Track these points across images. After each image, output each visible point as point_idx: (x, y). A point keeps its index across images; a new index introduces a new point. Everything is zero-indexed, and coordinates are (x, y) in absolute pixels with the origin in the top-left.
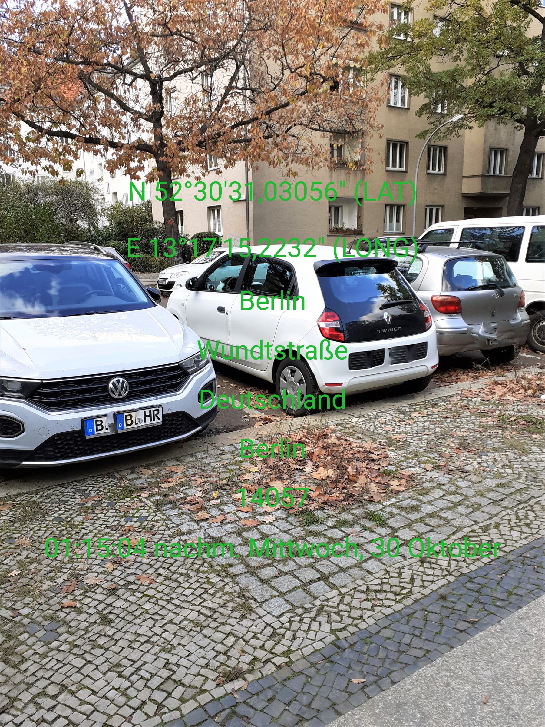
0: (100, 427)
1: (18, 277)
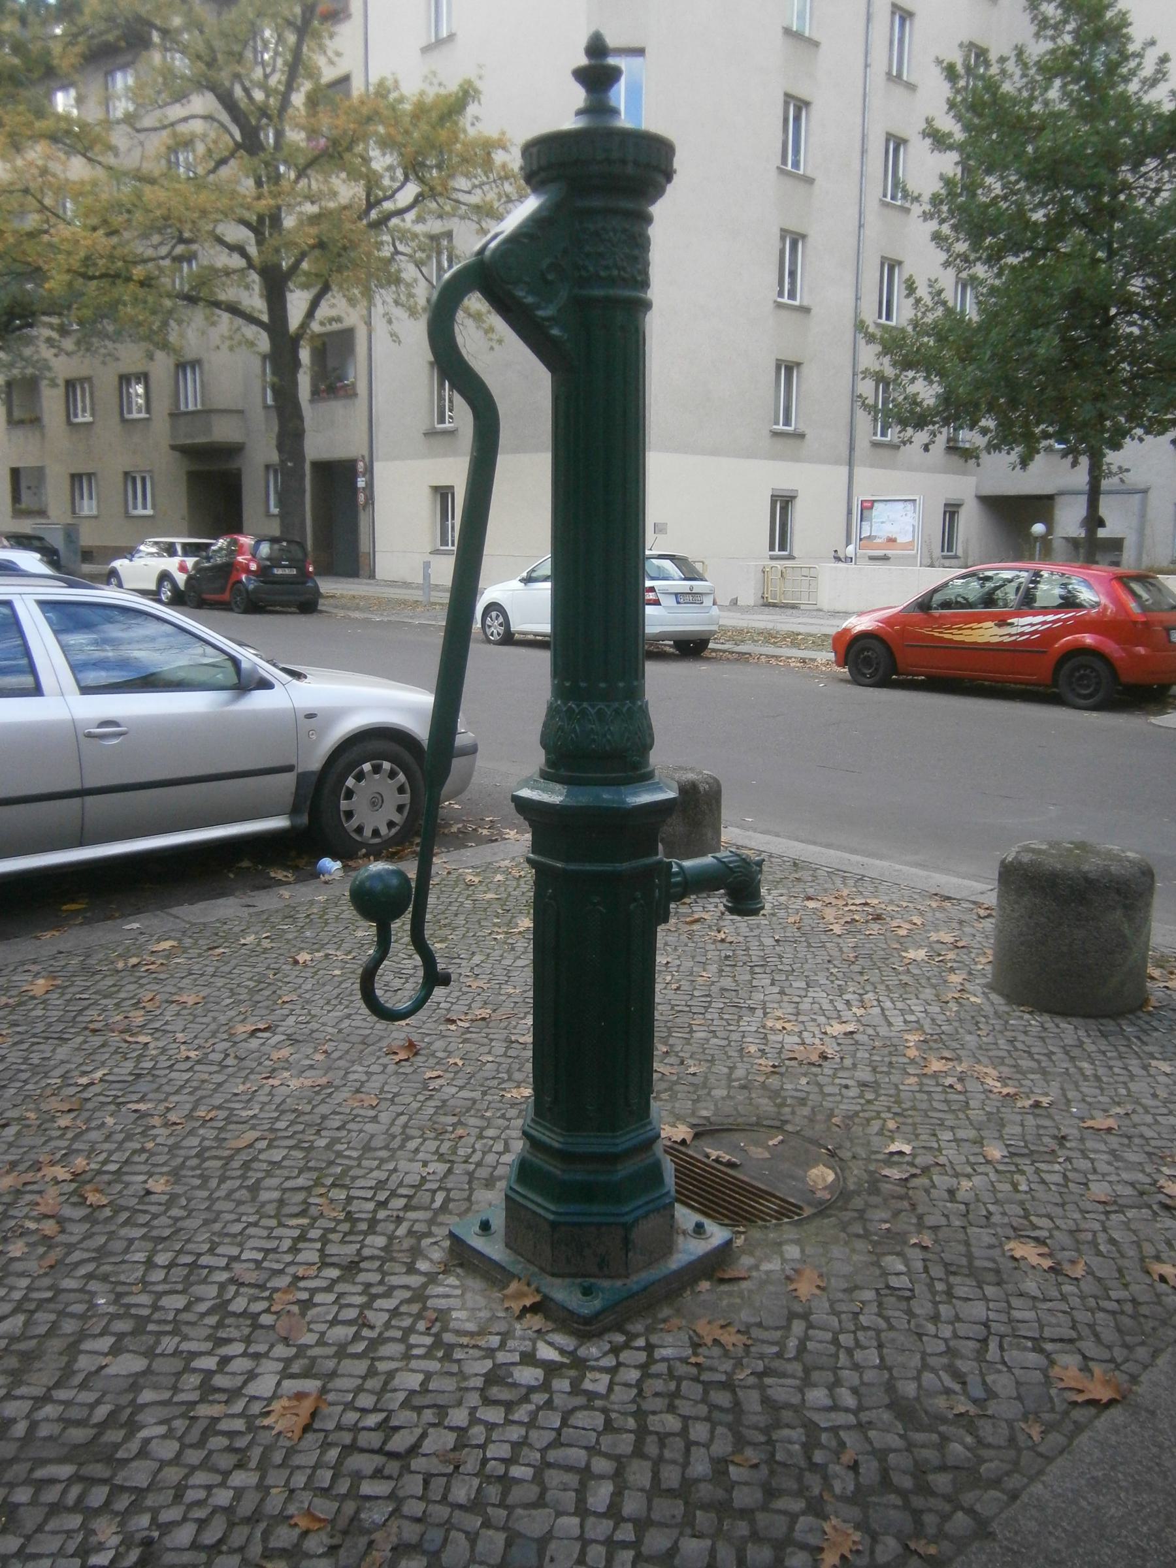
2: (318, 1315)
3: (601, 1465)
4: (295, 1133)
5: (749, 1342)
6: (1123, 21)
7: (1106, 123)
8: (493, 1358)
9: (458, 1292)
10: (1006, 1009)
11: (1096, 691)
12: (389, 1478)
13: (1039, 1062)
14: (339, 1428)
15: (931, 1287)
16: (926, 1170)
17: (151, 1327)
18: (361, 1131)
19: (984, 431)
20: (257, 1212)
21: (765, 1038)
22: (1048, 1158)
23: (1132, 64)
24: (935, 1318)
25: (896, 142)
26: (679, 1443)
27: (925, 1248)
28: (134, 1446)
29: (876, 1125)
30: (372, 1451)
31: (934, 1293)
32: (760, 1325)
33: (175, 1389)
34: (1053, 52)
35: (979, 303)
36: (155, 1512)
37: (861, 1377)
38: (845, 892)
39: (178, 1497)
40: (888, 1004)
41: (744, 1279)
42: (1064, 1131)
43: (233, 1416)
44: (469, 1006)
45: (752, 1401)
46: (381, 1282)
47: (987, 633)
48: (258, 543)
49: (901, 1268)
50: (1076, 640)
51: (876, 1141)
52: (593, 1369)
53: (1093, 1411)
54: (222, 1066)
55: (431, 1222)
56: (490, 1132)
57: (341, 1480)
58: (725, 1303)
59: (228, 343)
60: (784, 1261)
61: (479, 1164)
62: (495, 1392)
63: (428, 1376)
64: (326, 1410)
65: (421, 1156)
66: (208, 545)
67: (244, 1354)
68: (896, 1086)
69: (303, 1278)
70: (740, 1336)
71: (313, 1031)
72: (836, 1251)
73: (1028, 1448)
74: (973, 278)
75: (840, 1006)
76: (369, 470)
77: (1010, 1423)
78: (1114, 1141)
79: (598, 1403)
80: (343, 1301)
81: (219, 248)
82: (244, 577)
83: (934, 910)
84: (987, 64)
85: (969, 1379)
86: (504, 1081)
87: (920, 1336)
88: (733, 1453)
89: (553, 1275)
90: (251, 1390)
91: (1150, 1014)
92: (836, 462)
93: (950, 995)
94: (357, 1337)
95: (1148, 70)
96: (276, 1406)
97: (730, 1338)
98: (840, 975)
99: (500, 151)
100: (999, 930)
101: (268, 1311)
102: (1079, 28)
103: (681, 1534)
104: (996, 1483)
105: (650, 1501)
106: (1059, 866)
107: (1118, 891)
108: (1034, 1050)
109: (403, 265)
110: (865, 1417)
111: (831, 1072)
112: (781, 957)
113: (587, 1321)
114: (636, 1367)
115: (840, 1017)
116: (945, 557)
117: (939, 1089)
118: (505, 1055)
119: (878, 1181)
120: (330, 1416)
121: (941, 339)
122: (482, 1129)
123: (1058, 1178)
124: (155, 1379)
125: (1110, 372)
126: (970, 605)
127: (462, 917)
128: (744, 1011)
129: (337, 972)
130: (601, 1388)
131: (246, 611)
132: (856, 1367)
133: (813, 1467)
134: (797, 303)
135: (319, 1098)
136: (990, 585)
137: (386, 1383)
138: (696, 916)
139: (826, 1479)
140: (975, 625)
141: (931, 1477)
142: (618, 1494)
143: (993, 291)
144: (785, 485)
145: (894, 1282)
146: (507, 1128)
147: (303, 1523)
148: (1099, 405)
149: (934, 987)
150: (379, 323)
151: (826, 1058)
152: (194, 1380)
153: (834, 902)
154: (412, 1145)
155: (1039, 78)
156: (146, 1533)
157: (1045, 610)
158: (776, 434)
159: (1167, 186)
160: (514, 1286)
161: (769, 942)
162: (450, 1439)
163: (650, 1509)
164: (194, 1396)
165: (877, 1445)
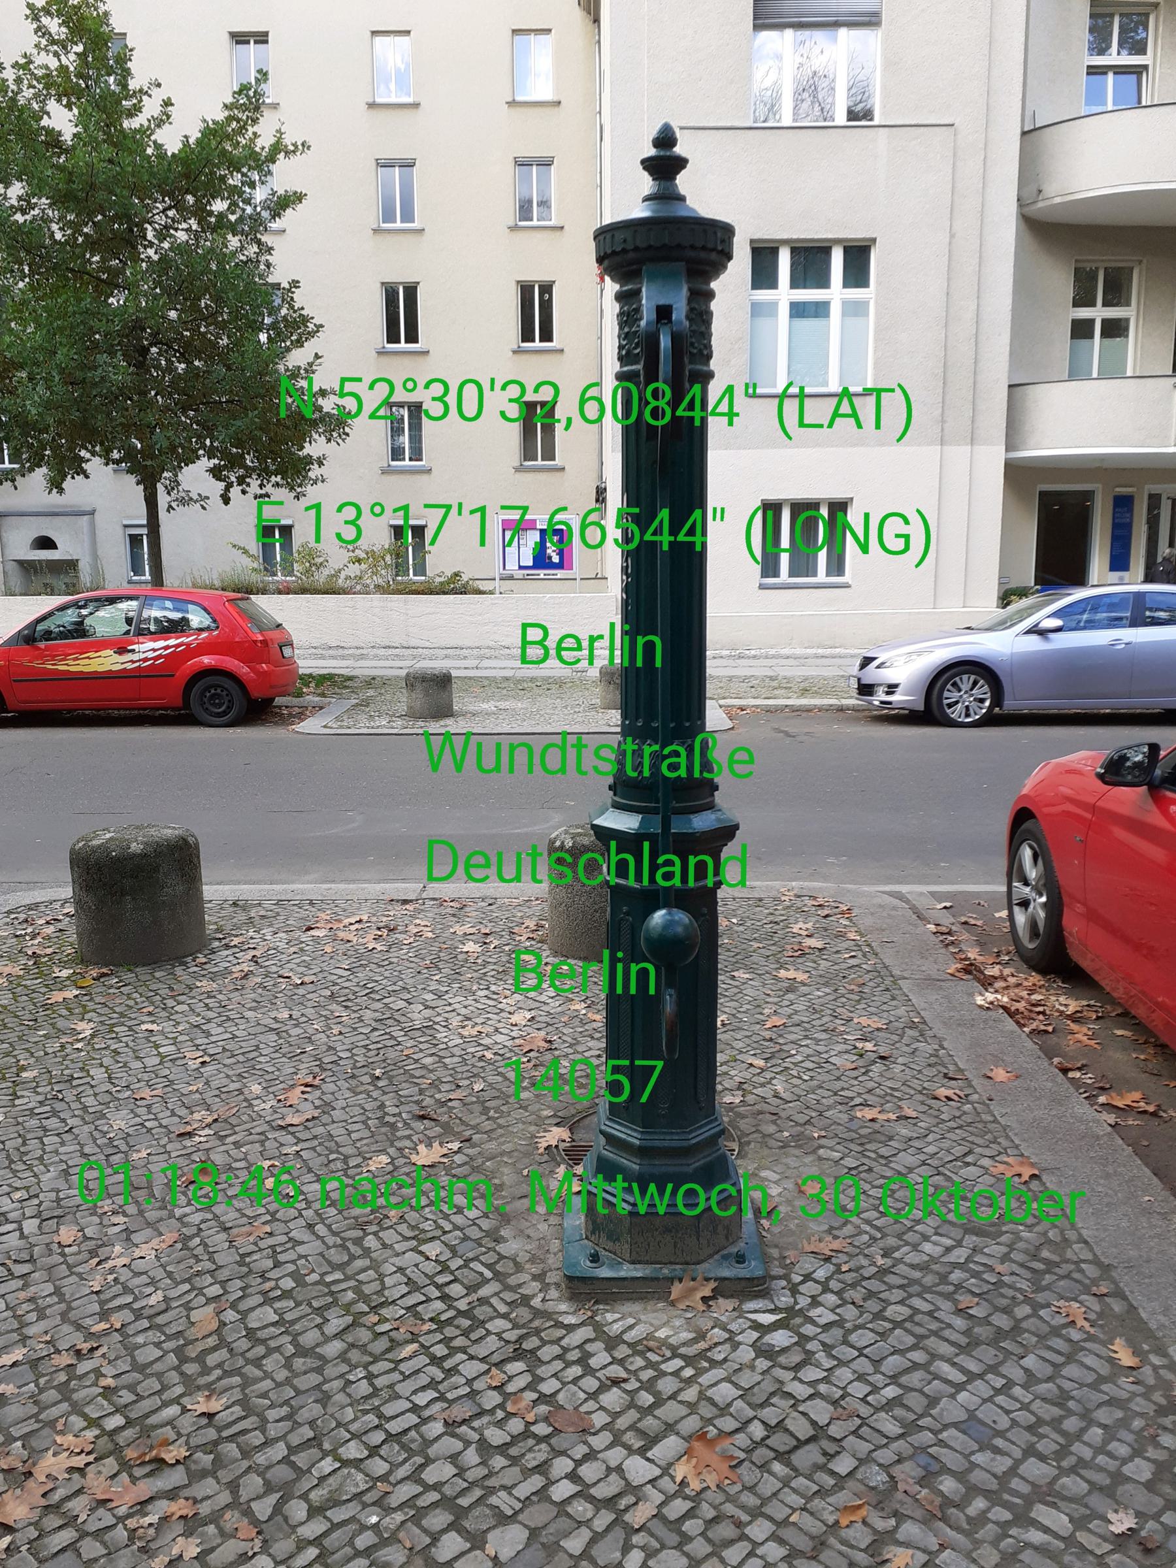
0: (534, 652)
1: (1121, 1336)
11: (229, 708)
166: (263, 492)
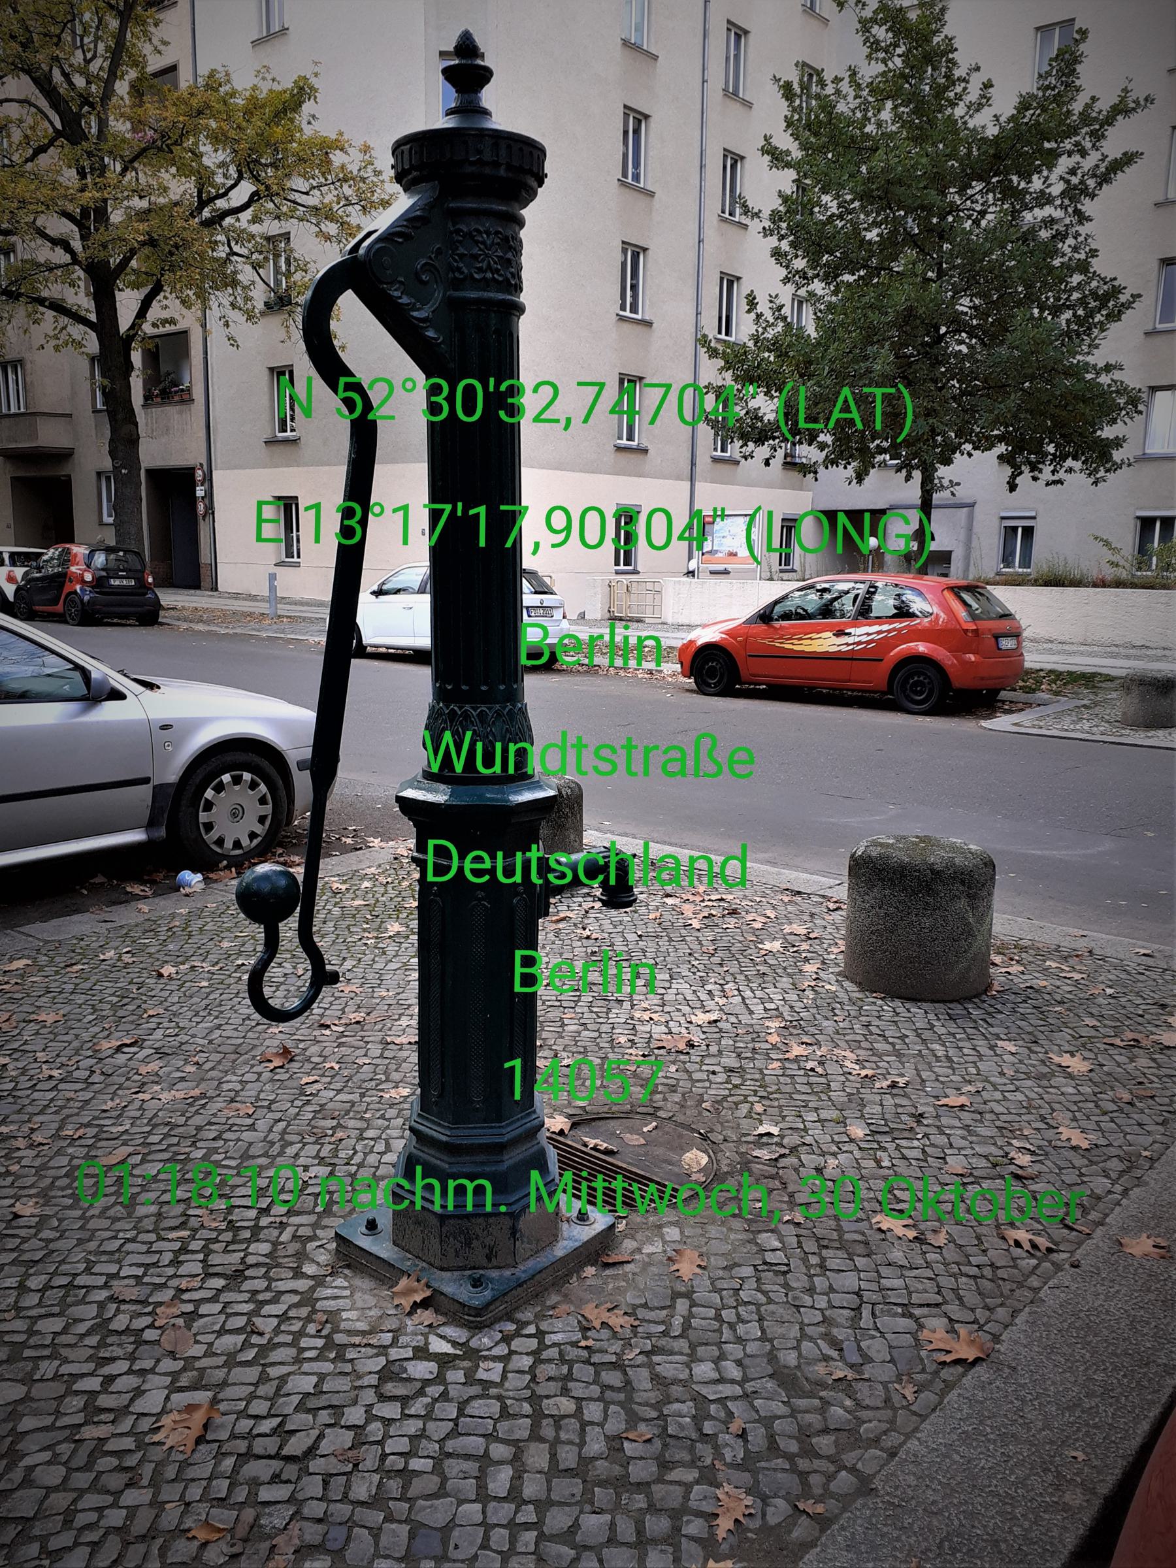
2: (205, 1326)
3: (499, 1451)
4: (170, 1146)
5: (637, 1323)
6: (950, 47)
7: (934, 145)
8: (386, 1355)
9: (347, 1293)
10: (860, 995)
12: (288, 1481)
13: (893, 1045)
14: (233, 1436)
15: (805, 1260)
16: (794, 1150)
17: (27, 1353)
18: (238, 1140)
19: (822, 446)
20: (135, 1228)
21: (634, 1028)
22: (907, 1134)
23: (959, 89)
24: (811, 1291)
25: (733, 160)
26: (574, 1424)
27: (798, 1224)
28: (17, 1475)
29: (744, 1108)
30: (270, 1457)
31: (808, 1267)
32: (645, 1306)
33: (58, 1413)
34: (884, 74)
35: (818, 318)
36: (44, 1539)
37: (744, 1349)
38: (701, 889)
39: (68, 1523)
40: (748, 993)
41: (628, 1262)
42: (921, 1110)
43: (122, 1435)
44: (343, 1010)
45: (642, 1379)
46: (268, 1289)
47: (825, 642)
48: (92, 552)
49: (777, 1244)
50: (909, 648)
51: (745, 1124)
52: (486, 1358)
53: (960, 1369)
54: (88, 1083)
55: (315, 1226)
56: (370, 1133)
57: (238, 1489)
58: (610, 1286)
59: (53, 342)
60: (665, 1242)
61: (360, 1165)
62: (390, 1388)
63: (322, 1377)
64: (219, 1420)
65: (301, 1161)
66: (42, 554)
67: (130, 1372)
68: (761, 1071)
69: (187, 1290)
70: (626, 1317)
71: (182, 1044)
72: (714, 1231)
73: (903, 1407)
74: (812, 294)
75: (703, 996)
76: (208, 479)
77: (885, 1385)
78: (967, 1118)
79: (493, 1391)
80: (229, 1311)
81: (39, 241)
82: (78, 588)
83: (786, 904)
84: (822, 84)
85: (845, 1345)
86: (382, 1082)
87: (797, 1307)
88: (626, 1430)
89: (442, 1269)
90: (139, 1406)
91: (994, 998)
92: (678, 478)
93: (806, 984)
94: (246, 1345)
95: (973, 95)
96: (166, 1420)
97: (617, 1320)
98: (701, 967)
99: (338, 152)
100: (851, 920)
101: (151, 1326)
102: (909, 51)
103: (581, 1512)
104: (876, 1441)
105: (549, 1482)
106: (906, 859)
107: (963, 882)
108: (887, 1033)
109: (239, 267)
110: (749, 1387)
111: (698, 1059)
112: (644, 951)
113: (478, 1311)
114: (527, 1354)
115: (703, 1006)
116: (782, 571)
117: (802, 1072)
118: (381, 1056)
119: (750, 1162)
120: (222, 1426)
121: (782, 355)
122: (362, 1130)
123: (917, 1153)
124: (34, 1405)
125: (941, 389)
126: (808, 616)
127: (331, 924)
128: (612, 1004)
129: (204, 984)
130: (495, 1377)
131: (82, 623)
132: (740, 1340)
133: (705, 1437)
134: (639, 317)
135: (193, 1109)
136: (827, 596)
137: (279, 1388)
138: (562, 915)
139: (716, 1448)
140: (814, 636)
141: (814, 1440)
142: (517, 1477)
143: (831, 307)
144: (629, 500)
145: (770, 1257)
146: (388, 1127)
147: (202, 1535)
148: (931, 421)
149: (790, 975)
150: (214, 325)
151: (692, 1046)
152: (78, 1402)
153: (692, 898)
154: (291, 1151)
155: (871, 99)
156: (37, 1562)
157: (879, 620)
158: (619, 449)
159: (991, 209)
160: (404, 1282)
161: (632, 937)
162: (348, 1437)
163: (549, 1490)
164: (79, 1419)
165: (762, 1414)
166: (1055, 478)
